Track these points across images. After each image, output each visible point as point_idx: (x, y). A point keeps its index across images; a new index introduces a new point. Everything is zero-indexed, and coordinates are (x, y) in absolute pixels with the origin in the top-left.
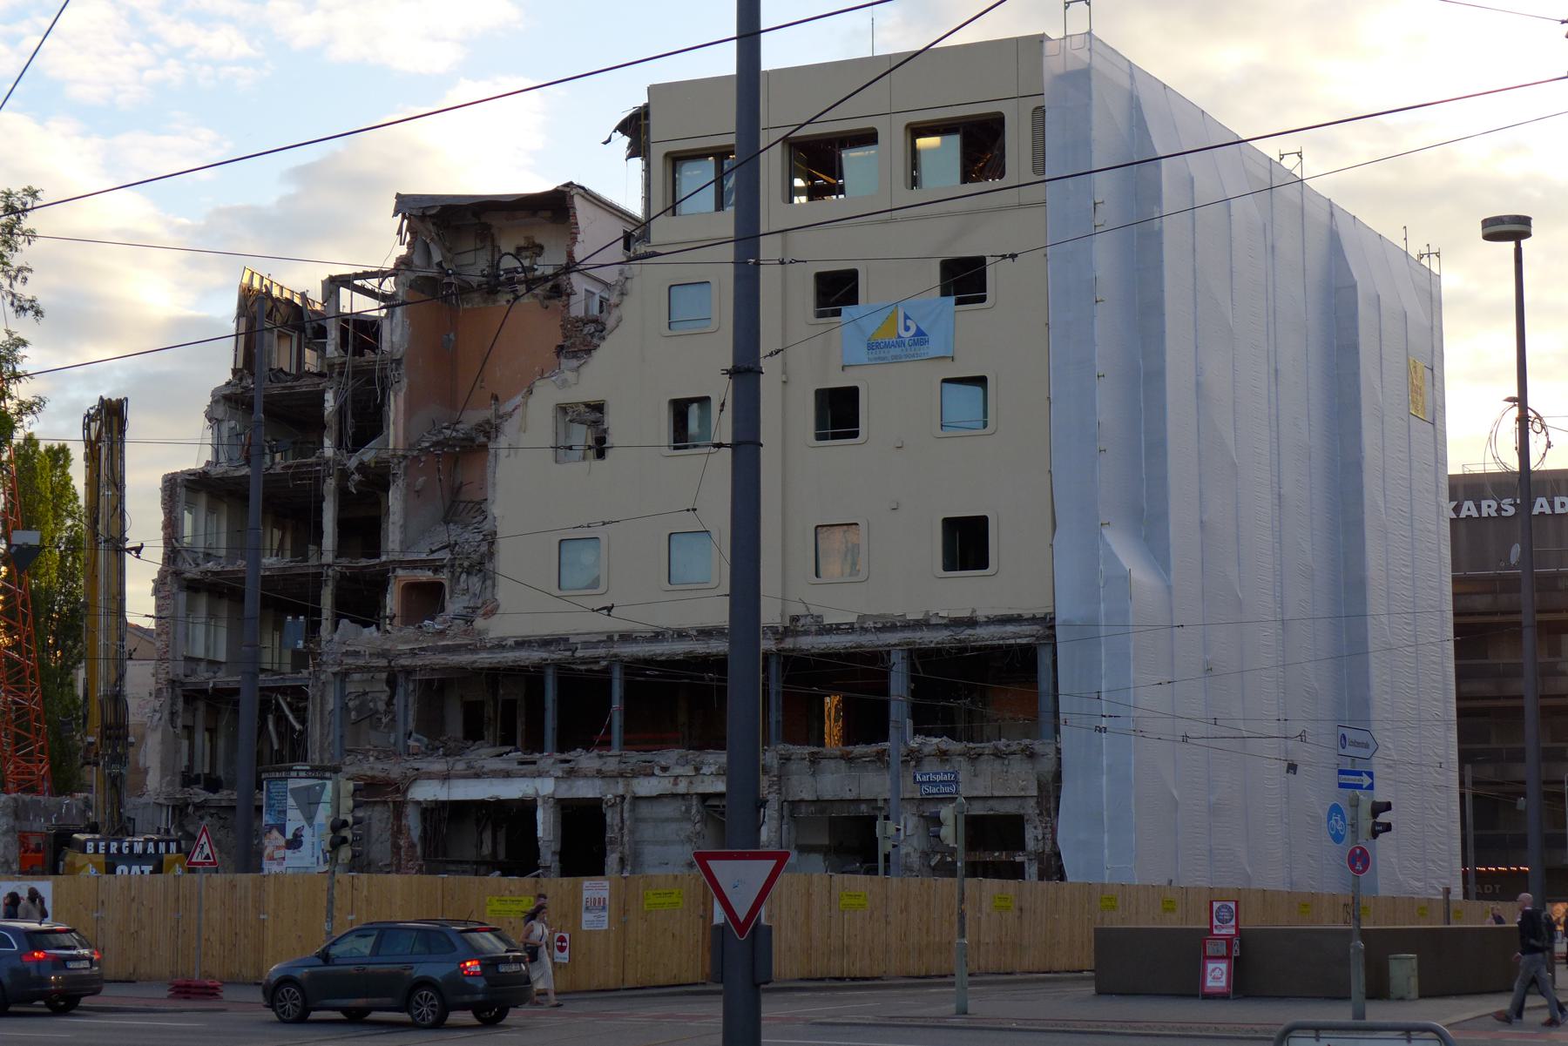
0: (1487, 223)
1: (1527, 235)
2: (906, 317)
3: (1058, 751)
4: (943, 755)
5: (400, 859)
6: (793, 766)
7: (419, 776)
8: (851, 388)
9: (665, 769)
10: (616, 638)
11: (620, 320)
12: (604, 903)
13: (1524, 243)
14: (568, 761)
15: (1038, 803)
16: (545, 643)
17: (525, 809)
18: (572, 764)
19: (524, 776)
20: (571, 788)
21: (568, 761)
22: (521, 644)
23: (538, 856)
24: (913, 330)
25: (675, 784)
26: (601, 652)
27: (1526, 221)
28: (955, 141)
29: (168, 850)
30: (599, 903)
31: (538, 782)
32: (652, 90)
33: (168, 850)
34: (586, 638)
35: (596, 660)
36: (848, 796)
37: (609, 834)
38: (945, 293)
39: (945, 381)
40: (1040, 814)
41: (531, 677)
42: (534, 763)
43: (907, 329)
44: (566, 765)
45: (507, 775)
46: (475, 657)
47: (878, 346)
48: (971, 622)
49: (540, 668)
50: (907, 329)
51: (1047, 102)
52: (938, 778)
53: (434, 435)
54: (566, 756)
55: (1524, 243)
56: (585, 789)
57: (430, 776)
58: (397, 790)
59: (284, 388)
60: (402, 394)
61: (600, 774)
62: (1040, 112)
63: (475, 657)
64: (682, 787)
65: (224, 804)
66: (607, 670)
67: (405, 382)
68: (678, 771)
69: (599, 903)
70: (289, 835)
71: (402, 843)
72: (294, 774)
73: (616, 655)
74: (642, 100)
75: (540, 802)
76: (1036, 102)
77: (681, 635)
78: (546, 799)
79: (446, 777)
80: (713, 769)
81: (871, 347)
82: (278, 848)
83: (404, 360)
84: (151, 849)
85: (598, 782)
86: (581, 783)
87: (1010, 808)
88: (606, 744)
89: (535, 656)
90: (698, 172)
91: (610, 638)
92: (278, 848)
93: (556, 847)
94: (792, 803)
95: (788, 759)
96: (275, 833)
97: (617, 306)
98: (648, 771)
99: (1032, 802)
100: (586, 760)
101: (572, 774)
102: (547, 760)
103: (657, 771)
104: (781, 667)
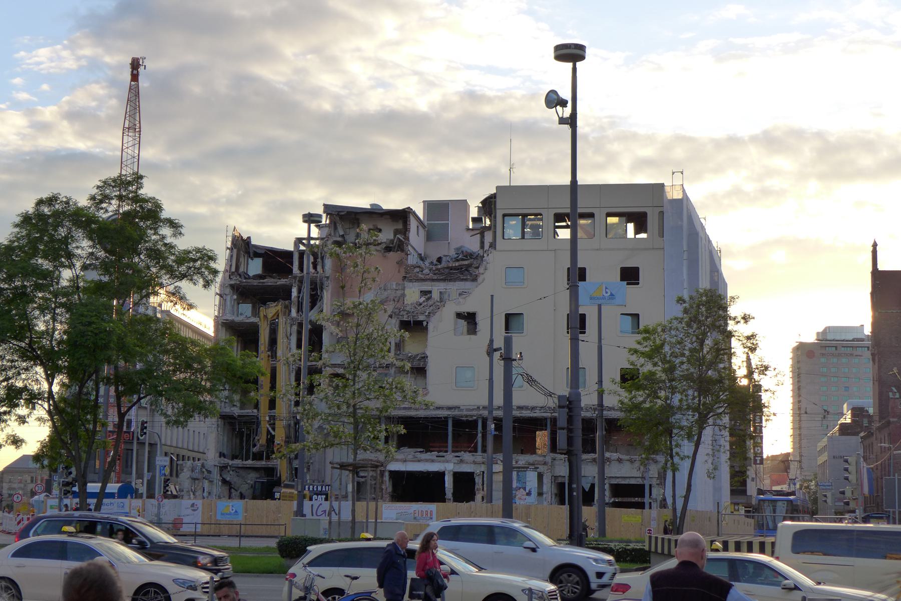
0: (558, 48)
1: (582, 58)
2: (606, 288)
4: (620, 461)
5: (383, 494)
6: (557, 462)
11: (484, 280)
12: (431, 514)
13: (579, 64)
14: (459, 457)
16: (450, 408)
17: (441, 475)
18: (461, 458)
19: (440, 462)
21: (459, 457)
23: (445, 494)
26: (475, 413)
27: (582, 48)
30: (427, 514)
31: (446, 465)
32: (497, 188)
34: (468, 407)
35: (472, 416)
37: (477, 487)
38: (622, 279)
39: (621, 314)
41: (443, 422)
42: (444, 457)
43: (607, 293)
44: (458, 458)
45: (433, 461)
46: (418, 413)
47: (594, 298)
49: (446, 418)
50: (607, 293)
51: (665, 209)
52: (826, 484)
54: (457, 454)
55: (578, 64)
58: (382, 465)
59: (259, 283)
60: (330, 291)
61: (475, 463)
62: (662, 213)
63: (418, 413)
65: (240, 466)
66: (476, 422)
67: (330, 287)
69: (427, 514)
70: (527, 491)
71: (383, 487)
72: (529, 469)
73: (481, 415)
74: (494, 191)
75: (446, 473)
76: (660, 209)
78: (449, 471)
81: (591, 298)
82: (523, 495)
83: (330, 278)
85: (472, 466)
88: (476, 451)
89: (444, 413)
90: (514, 222)
91: (478, 408)
92: (523, 495)
93: (452, 491)
94: (555, 477)
95: (555, 459)
96: (522, 490)
97: (483, 274)
98: (495, 462)
100: (467, 456)
101: (462, 461)
102: (450, 455)
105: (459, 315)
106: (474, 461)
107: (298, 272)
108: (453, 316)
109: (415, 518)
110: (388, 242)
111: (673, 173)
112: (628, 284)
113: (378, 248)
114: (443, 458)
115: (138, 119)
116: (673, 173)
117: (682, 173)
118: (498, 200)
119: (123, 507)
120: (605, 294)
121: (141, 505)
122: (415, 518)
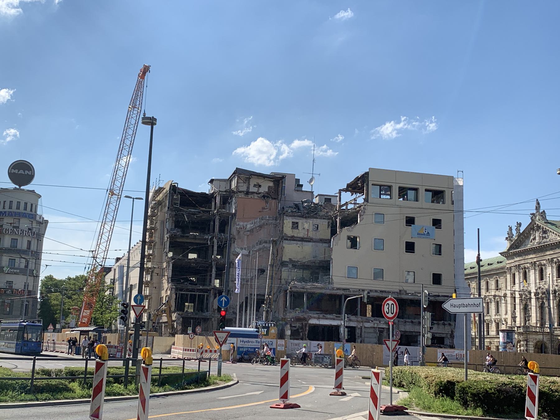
2: (425, 229)
3: (455, 325)
7: (311, 318)
8: (413, 242)
9: (372, 321)
10: (361, 290)
15: (450, 335)
16: (344, 289)
17: (337, 327)
19: (338, 320)
20: (349, 324)
22: (338, 289)
24: (427, 232)
25: (374, 325)
28: (431, 193)
29: (271, 325)
33: (271, 325)
36: (412, 331)
40: (451, 337)
42: (340, 317)
43: (426, 232)
45: (334, 319)
48: (439, 296)
50: (426, 232)
53: (82, 344)
56: (352, 324)
57: (315, 318)
61: (357, 321)
64: (376, 326)
68: (375, 322)
77: (376, 291)
79: (319, 318)
80: (383, 322)
82: (511, 347)
84: (267, 325)
86: (351, 323)
87: (443, 336)
96: (511, 344)
99: (449, 335)
100: (353, 318)
101: (350, 320)
103: (370, 321)
104: (478, 290)
105: (349, 238)
106: (357, 321)
107: (39, 219)
108: (346, 238)
109: (457, 358)
110: (265, 193)
111: (458, 171)
112: (436, 228)
113: (259, 195)
114: (339, 318)
115: (134, 96)
116: (458, 171)
117: (462, 172)
118: (370, 174)
119: (272, 344)
120: (425, 233)
121: (284, 343)
122: (457, 358)
